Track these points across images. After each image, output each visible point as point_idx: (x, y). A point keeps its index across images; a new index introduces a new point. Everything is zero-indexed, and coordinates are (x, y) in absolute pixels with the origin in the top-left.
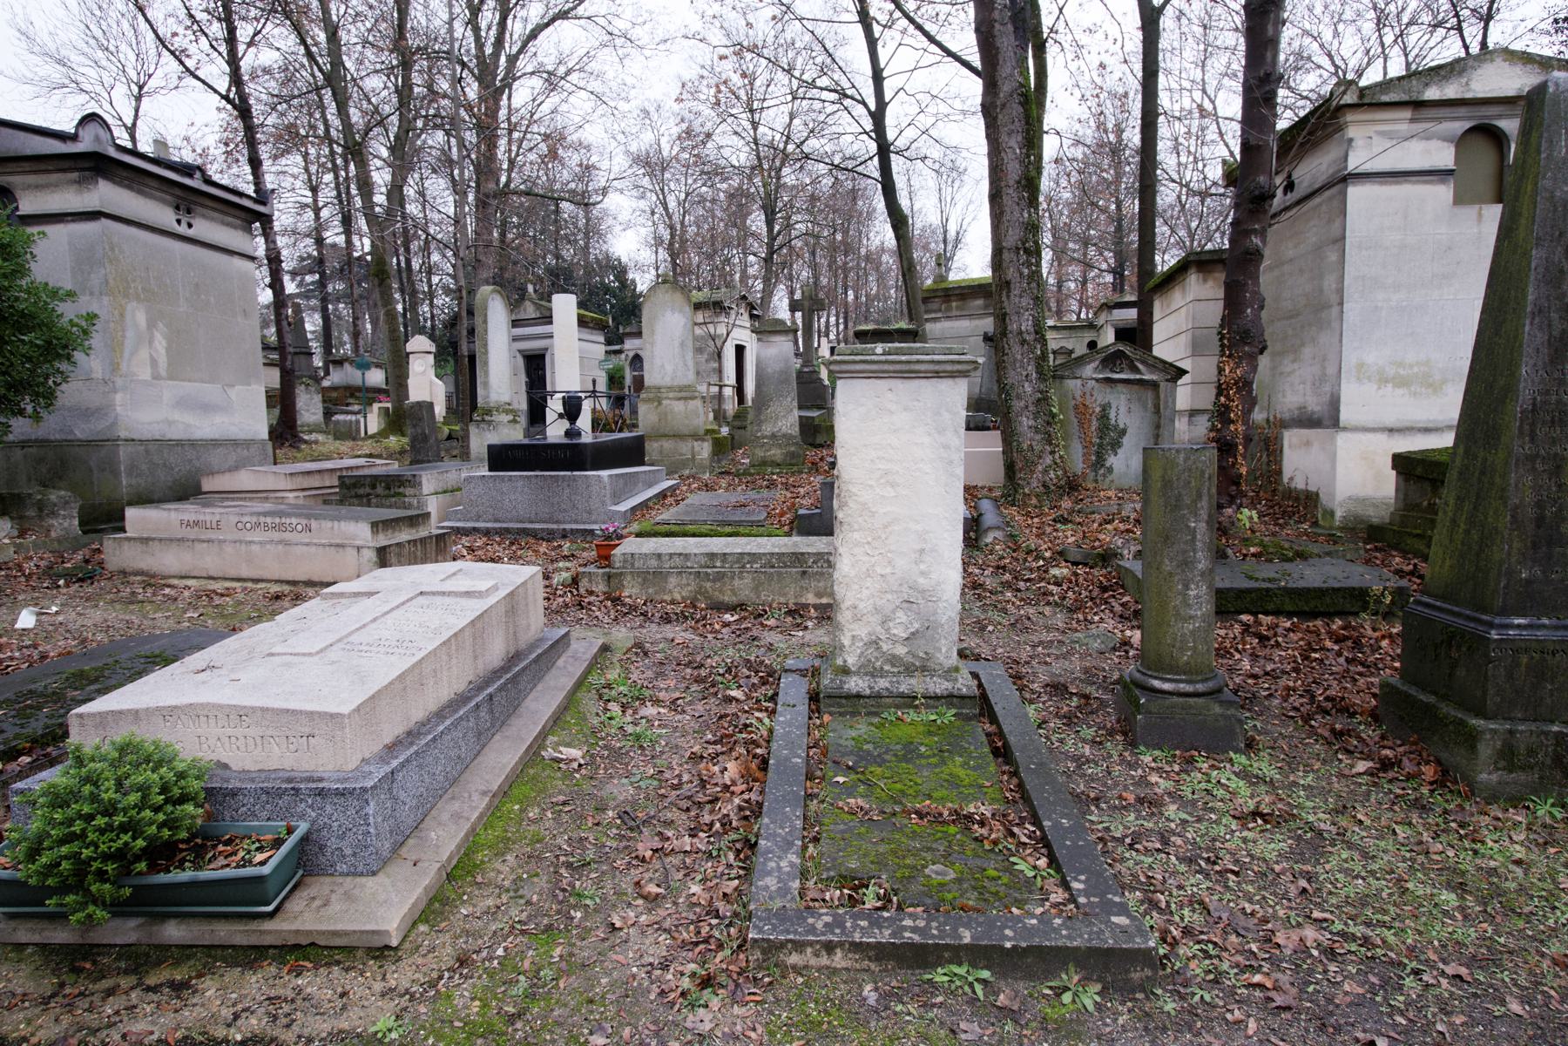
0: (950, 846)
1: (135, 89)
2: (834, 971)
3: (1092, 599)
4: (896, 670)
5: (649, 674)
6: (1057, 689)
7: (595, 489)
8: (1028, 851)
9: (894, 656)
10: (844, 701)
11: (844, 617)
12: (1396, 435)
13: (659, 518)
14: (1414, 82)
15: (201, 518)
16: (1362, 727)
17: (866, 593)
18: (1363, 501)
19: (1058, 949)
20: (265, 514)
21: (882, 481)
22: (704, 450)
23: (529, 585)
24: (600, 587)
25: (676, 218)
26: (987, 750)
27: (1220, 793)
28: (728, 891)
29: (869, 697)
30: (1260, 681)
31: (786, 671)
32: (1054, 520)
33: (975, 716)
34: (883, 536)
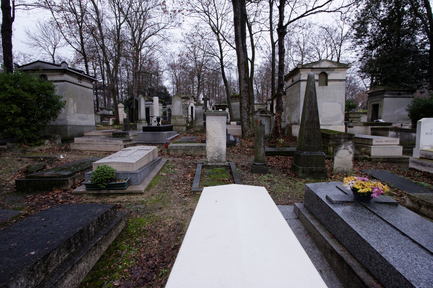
1: (54, 46)
6: (243, 166)
15: (89, 140)
20: (101, 139)
22: (184, 129)
25: (178, 78)
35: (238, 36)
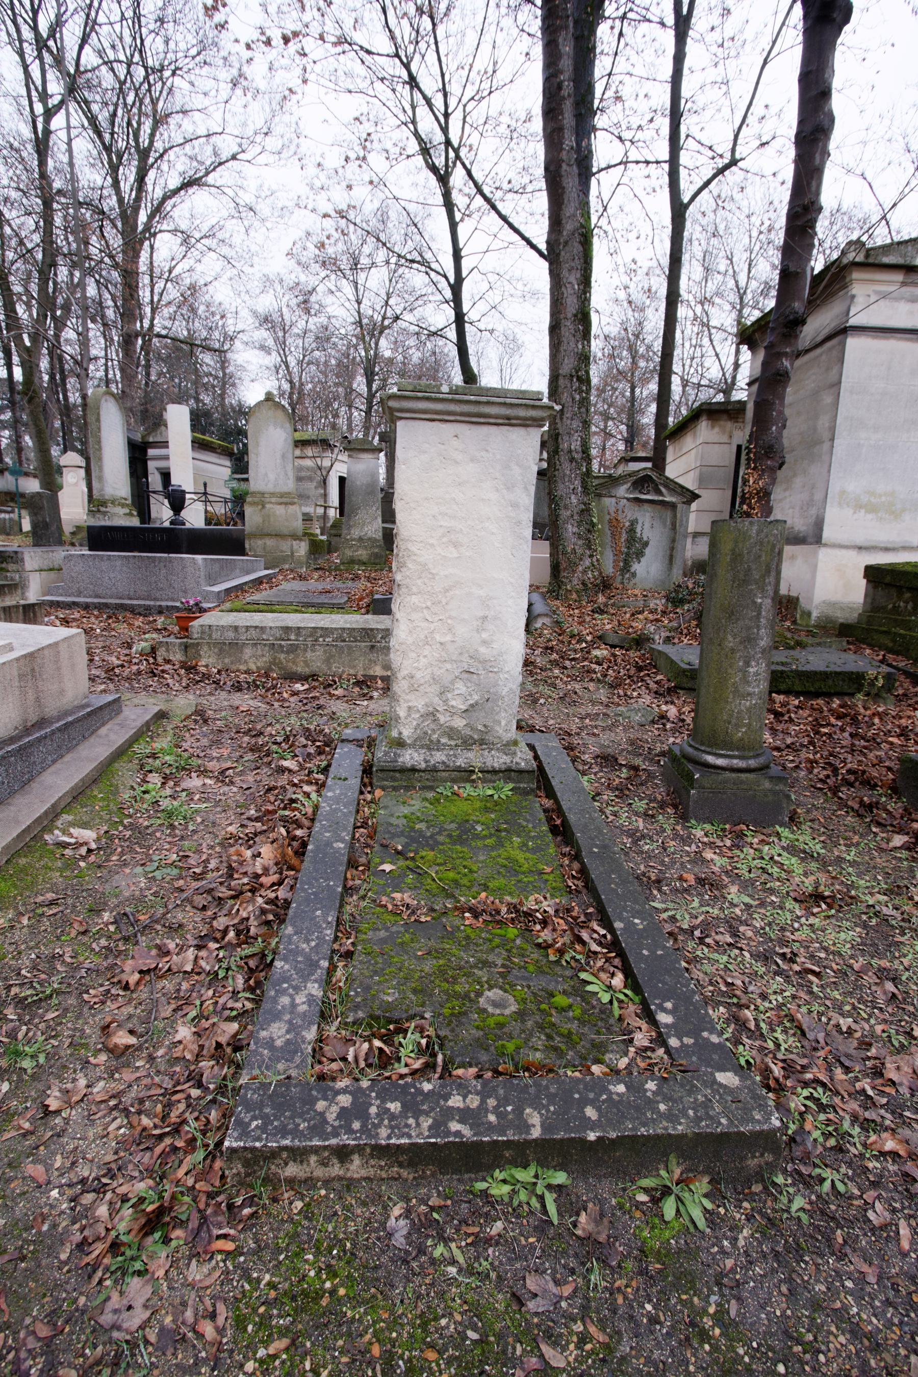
0: (509, 958)
2: (350, 1184)
3: (630, 677)
4: (453, 743)
5: (205, 742)
6: (607, 760)
7: (190, 570)
8: (600, 963)
9: (452, 729)
10: (398, 775)
11: (400, 687)
12: (864, 552)
13: (248, 599)
14: (910, 248)
16: (884, 799)
17: (423, 661)
18: (833, 604)
19: (658, 1137)
21: (445, 540)
22: (302, 549)
23: (63, 648)
24: (177, 656)
26: (545, 828)
27: (775, 870)
28: (223, 1040)
29: (424, 771)
30: (784, 753)
31: (343, 741)
32: (593, 611)
33: (532, 790)
34: (444, 601)
35: (560, 87)
